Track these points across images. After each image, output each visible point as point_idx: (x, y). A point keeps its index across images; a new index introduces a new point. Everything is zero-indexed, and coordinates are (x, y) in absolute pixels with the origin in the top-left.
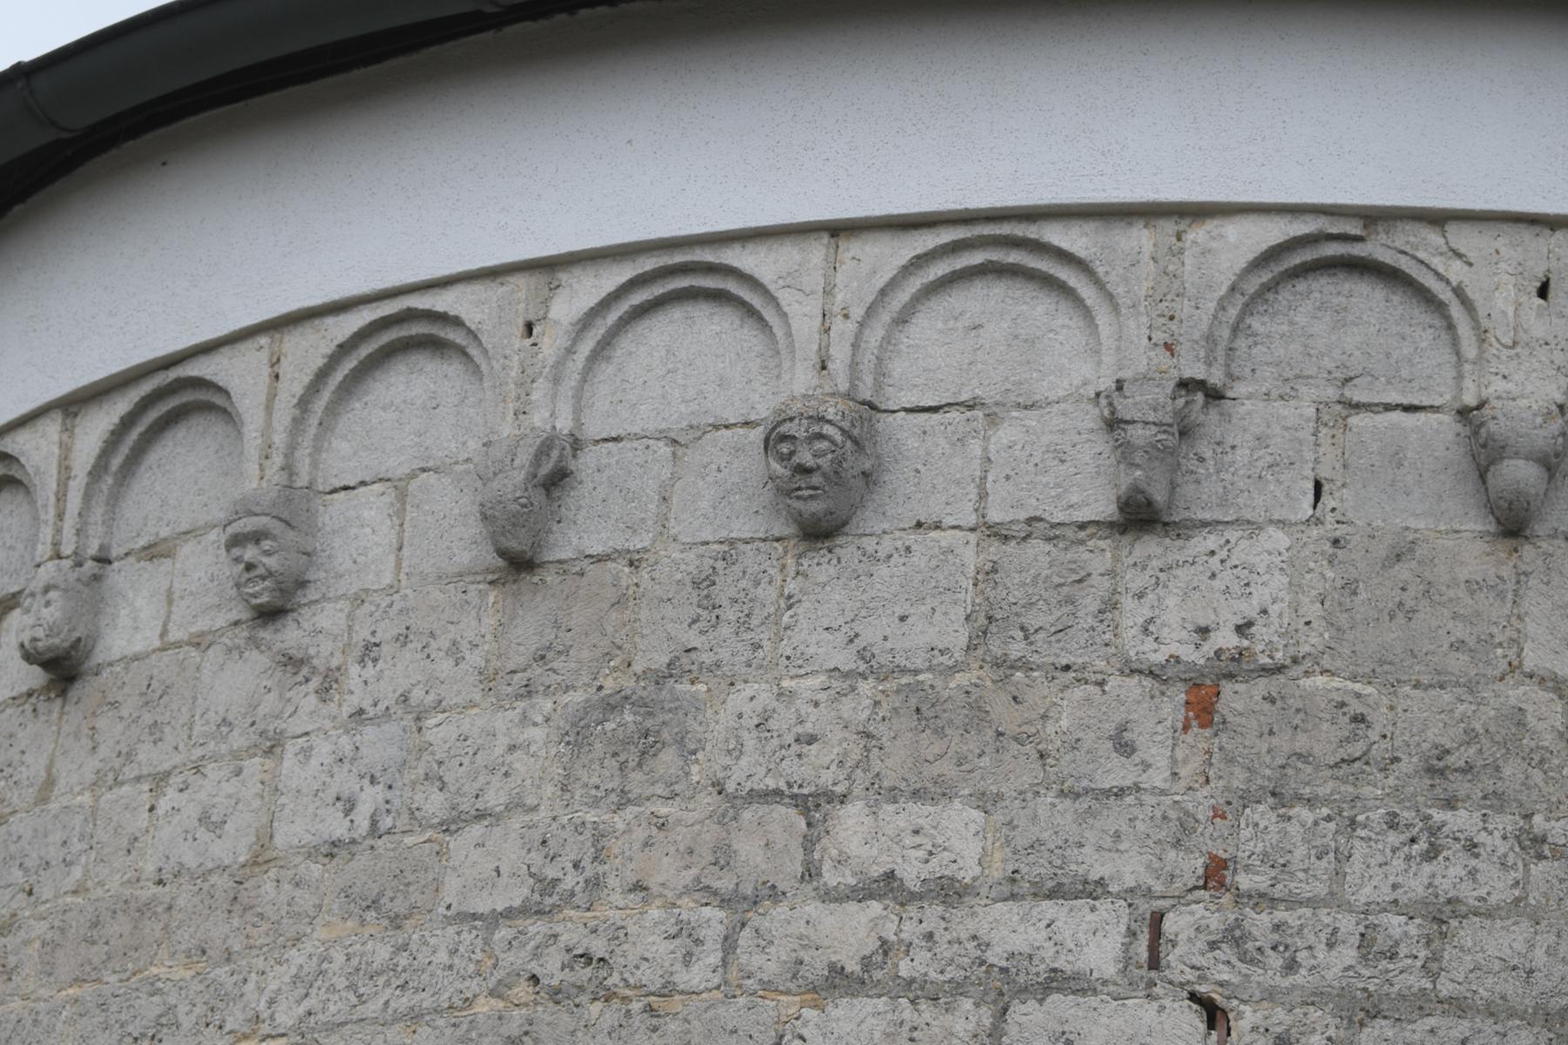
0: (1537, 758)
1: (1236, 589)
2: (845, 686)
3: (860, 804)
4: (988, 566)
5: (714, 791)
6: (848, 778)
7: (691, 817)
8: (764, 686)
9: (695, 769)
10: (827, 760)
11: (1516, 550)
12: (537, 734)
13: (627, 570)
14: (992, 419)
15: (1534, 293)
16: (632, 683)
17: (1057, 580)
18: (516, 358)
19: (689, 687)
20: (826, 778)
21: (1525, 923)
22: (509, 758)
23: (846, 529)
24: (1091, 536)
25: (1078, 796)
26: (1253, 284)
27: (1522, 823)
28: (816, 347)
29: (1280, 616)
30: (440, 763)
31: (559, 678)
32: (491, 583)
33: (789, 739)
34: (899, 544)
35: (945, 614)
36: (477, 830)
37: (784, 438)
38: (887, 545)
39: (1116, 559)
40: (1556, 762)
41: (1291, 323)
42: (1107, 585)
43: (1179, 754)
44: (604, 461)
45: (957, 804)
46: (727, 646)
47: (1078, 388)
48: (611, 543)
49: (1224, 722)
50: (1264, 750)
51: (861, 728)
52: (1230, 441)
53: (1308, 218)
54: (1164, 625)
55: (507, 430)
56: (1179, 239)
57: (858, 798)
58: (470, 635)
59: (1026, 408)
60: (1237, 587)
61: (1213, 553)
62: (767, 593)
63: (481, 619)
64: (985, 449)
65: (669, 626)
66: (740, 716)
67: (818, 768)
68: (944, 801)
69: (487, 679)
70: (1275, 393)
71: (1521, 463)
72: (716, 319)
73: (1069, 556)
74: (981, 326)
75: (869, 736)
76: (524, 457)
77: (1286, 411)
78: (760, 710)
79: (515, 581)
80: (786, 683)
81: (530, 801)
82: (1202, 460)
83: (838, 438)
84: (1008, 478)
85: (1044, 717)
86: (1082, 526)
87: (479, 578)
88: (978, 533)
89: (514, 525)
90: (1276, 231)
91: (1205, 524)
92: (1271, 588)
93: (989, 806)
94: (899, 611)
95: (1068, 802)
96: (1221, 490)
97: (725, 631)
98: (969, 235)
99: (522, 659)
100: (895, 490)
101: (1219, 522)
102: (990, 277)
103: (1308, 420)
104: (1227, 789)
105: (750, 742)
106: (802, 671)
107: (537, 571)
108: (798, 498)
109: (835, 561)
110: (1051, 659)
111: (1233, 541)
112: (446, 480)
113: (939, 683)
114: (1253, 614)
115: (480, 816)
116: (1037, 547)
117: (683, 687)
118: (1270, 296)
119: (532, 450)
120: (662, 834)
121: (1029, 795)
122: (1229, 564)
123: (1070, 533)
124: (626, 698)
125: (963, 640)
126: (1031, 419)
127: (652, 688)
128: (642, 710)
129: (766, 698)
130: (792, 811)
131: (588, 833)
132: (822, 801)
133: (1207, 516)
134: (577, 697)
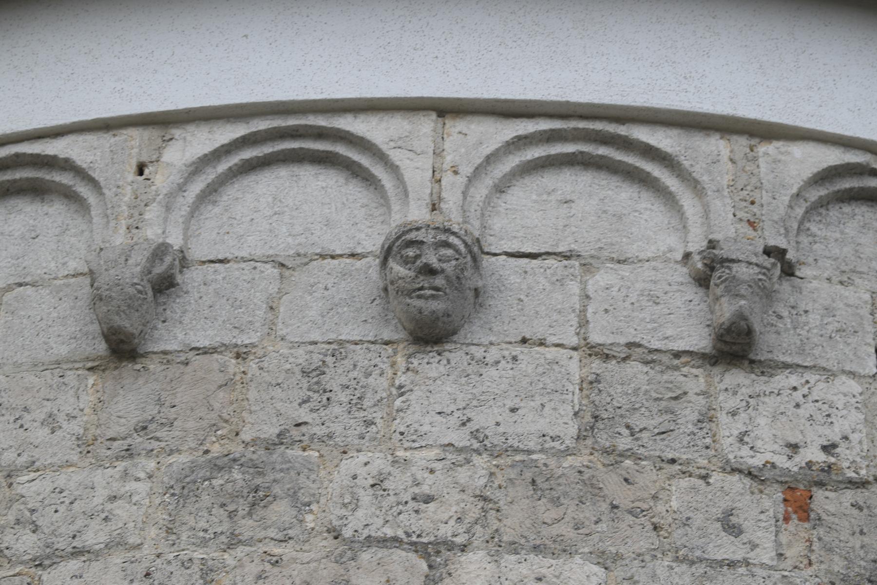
1: (819, 417)
2: (460, 458)
3: (481, 553)
4: (592, 377)
5: (330, 537)
6: (468, 532)
7: (306, 557)
8: (377, 455)
9: (309, 518)
10: (445, 517)
12: (142, 487)
13: (234, 361)
14: (587, 267)
16: (241, 448)
17: (655, 395)
18: (129, 187)
19: (301, 453)
20: (446, 531)
22: (109, 506)
23: (455, 338)
24: (685, 364)
25: (692, 563)
26: (814, 195)
28: (429, 191)
29: (860, 442)
30: (33, 511)
31: (163, 444)
32: (90, 369)
33: (407, 497)
34: (506, 353)
35: (555, 409)
36: (74, 565)
37: (411, 243)
38: (494, 354)
39: (709, 384)
41: (842, 233)
42: (703, 402)
43: (784, 538)
44: (210, 277)
45: (577, 559)
46: (340, 421)
47: (664, 253)
48: (218, 339)
49: (819, 519)
50: (858, 546)
51: (478, 492)
52: (802, 306)
53: (857, 152)
54: (757, 438)
55: (120, 239)
56: (752, 150)
57: (478, 548)
58: (68, 409)
59: (619, 262)
60: (820, 417)
61: (795, 389)
62: (380, 383)
63: (80, 398)
64: (584, 289)
65: (279, 405)
66: (355, 477)
67: (438, 521)
68: (564, 556)
69: (86, 444)
70: (835, 279)
72: (321, 177)
73: (665, 377)
74: (572, 201)
75: (485, 499)
76: (139, 258)
77: (847, 292)
78: (375, 473)
79: (116, 368)
80: (400, 453)
81: (133, 540)
82: (780, 317)
83: (462, 248)
84: (606, 311)
85: (655, 497)
86: (677, 355)
87: (77, 365)
88: (580, 352)
89: (129, 306)
90: (834, 157)
91: (786, 366)
92: (849, 421)
93: (609, 563)
94: (510, 404)
95: (684, 567)
96: (799, 342)
97: (336, 410)
98: (565, 126)
99: (123, 429)
100: (500, 313)
101: (798, 366)
102: (578, 168)
103: (866, 302)
104: (828, 572)
105: (366, 498)
106: (417, 445)
107: (139, 360)
108: (419, 297)
109: (445, 362)
110: (658, 453)
111: (812, 382)
112: (44, 292)
113: (552, 462)
114: (837, 439)
115: (77, 553)
116: (634, 368)
117: (295, 453)
118: (823, 211)
119: (147, 254)
120: (276, 570)
121: (647, 558)
122: (810, 398)
123: (666, 359)
124: (235, 460)
125: (573, 430)
126: (625, 270)
127: (262, 452)
128: (251, 470)
129: (380, 462)
130: (412, 556)
131: (196, 568)
132: (442, 549)
133: (788, 359)
134: (183, 459)
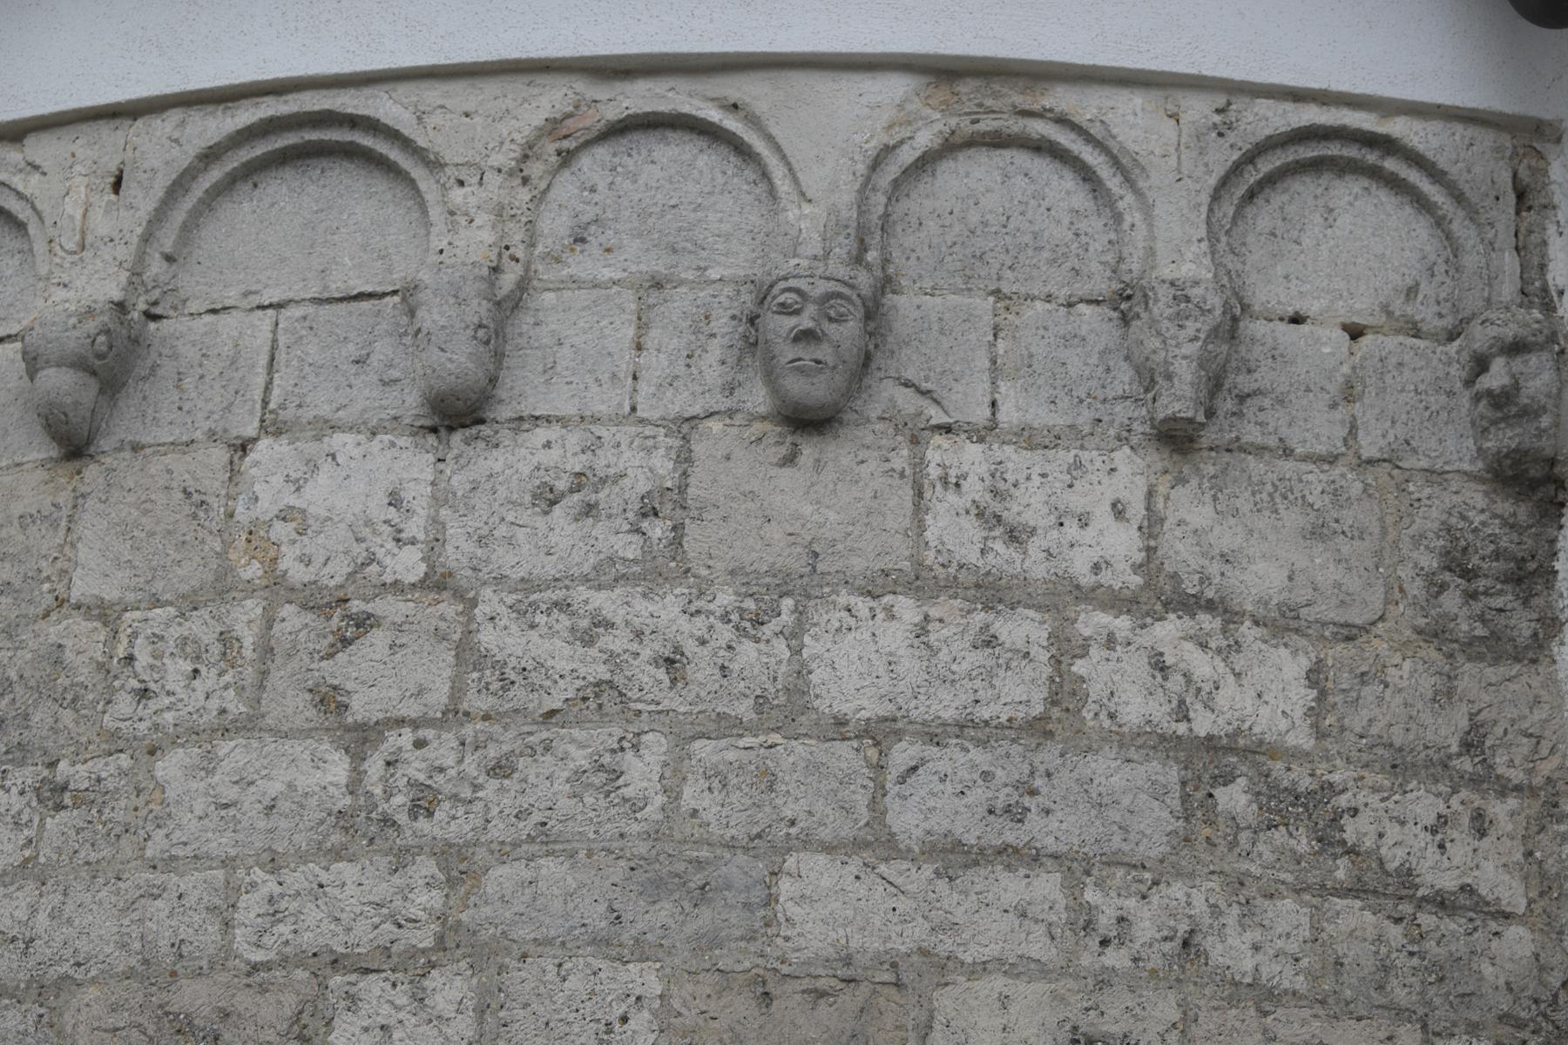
0: (69, 697)
11: (79, 473)
15: (109, 189)
21: (31, 886)
27: (46, 773)
40: (91, 697)
71: (51, 371)
